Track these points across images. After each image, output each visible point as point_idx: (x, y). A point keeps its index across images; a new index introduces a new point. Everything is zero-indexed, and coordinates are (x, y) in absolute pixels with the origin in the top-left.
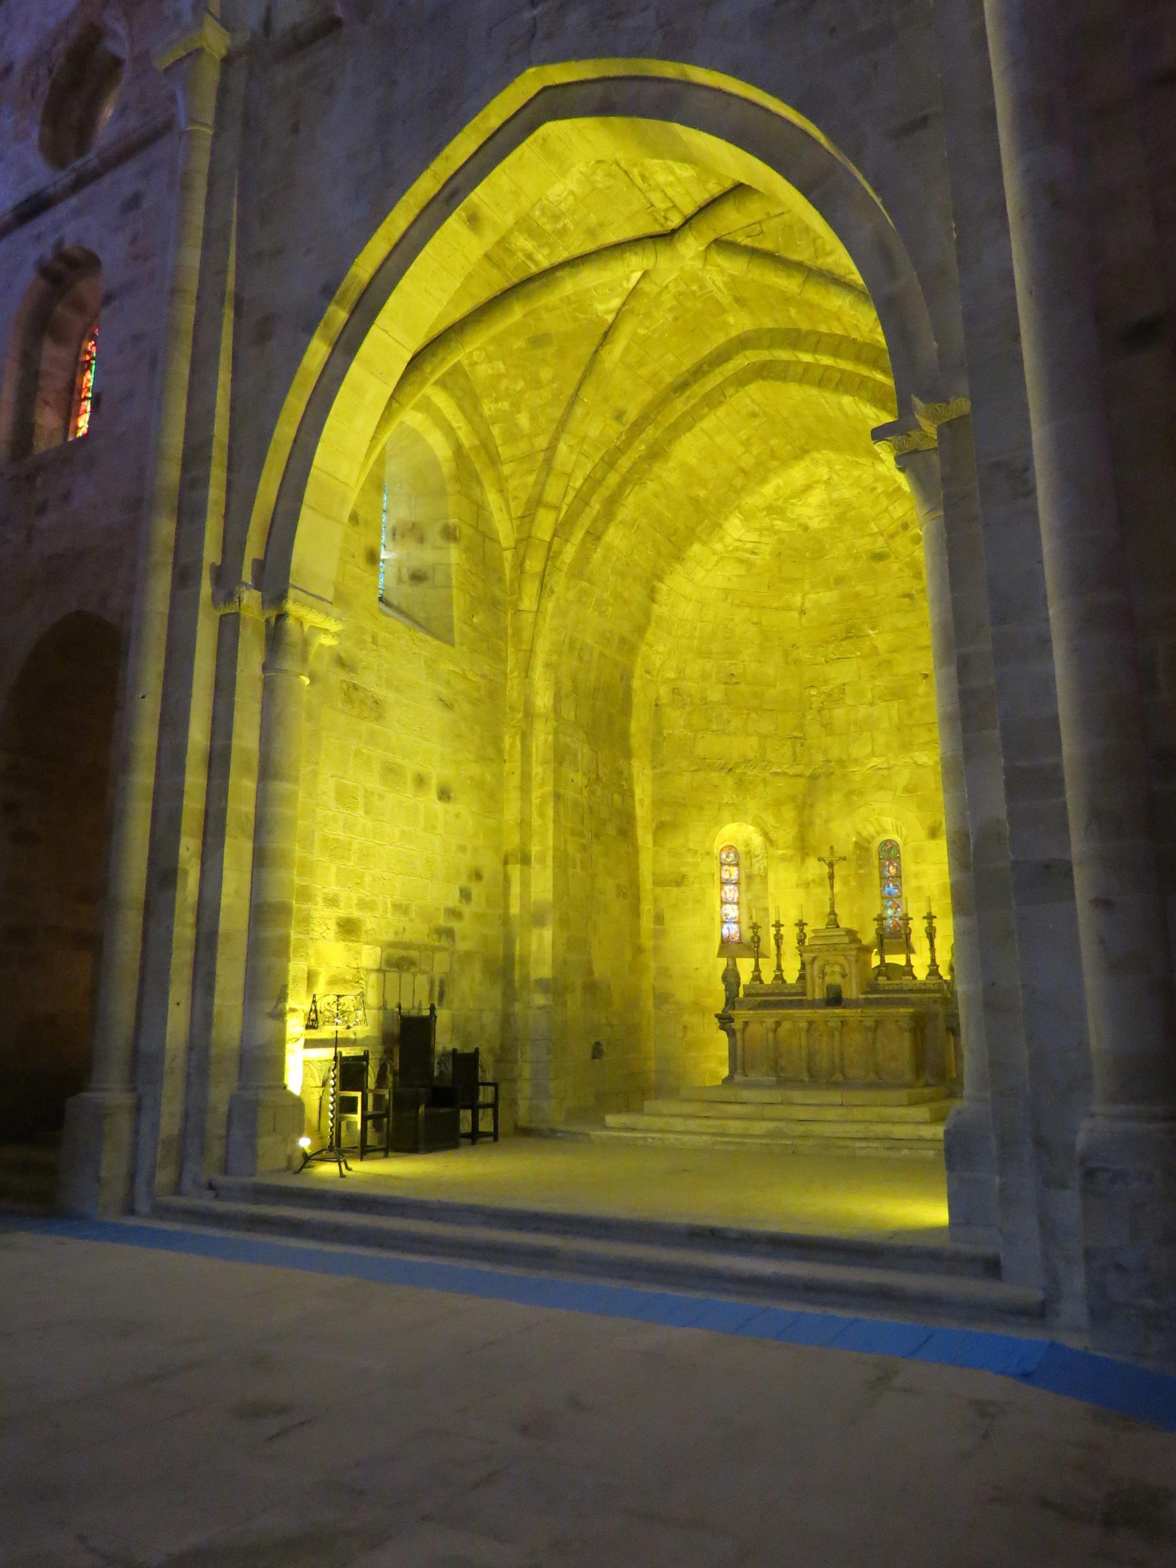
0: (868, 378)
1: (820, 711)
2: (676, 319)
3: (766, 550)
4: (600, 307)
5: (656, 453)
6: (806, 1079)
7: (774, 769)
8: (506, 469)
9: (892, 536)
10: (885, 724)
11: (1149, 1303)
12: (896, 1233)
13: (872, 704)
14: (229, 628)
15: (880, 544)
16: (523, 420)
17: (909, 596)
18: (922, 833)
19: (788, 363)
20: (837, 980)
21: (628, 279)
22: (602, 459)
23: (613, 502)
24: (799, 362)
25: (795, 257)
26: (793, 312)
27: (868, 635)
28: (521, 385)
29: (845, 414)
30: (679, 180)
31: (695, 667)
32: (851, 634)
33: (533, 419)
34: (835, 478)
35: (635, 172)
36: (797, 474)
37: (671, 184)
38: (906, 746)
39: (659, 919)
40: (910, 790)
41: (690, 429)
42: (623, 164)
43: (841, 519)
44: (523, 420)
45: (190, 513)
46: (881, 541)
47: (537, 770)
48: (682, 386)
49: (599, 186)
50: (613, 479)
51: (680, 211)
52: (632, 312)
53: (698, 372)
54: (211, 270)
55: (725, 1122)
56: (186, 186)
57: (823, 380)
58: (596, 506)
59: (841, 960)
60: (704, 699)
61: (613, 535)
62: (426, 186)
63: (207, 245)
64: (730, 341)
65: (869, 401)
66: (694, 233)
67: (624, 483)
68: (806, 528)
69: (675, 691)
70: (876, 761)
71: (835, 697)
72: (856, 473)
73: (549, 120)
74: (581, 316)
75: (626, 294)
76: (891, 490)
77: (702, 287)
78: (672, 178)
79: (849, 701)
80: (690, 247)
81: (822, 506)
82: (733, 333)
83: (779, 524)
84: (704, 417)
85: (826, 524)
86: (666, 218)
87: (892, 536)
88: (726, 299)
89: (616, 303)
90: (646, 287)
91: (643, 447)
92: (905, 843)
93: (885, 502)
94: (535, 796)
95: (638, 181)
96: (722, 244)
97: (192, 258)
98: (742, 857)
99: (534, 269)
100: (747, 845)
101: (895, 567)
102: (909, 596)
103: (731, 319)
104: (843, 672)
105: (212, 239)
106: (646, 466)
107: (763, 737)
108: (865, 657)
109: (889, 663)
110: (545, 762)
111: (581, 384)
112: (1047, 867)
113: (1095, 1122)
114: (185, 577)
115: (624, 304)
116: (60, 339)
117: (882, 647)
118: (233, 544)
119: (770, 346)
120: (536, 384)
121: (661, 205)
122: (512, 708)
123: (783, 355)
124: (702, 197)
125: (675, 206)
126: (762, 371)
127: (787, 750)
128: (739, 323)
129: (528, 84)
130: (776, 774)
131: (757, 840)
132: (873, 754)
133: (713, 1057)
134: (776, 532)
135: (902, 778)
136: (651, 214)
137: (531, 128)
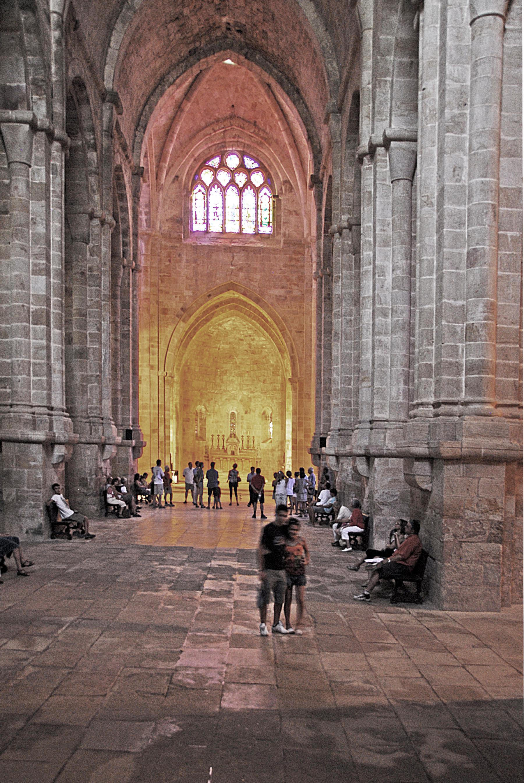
5: (207, 320)
10: (236, 382)
18: (244, 412)
20: (233, 450)
23: (196, 329)
32: (231, 357)
38: (241, 389)
40: (241, 401)
43: (234, 329)
67: (199, 325)
70: (233, 392)
81: (230, 324)
92: (238, 414)
107: (206, 382)
110: (176, 394)
117: (238, 362)
126: (236, 308)
135: (240, 398)
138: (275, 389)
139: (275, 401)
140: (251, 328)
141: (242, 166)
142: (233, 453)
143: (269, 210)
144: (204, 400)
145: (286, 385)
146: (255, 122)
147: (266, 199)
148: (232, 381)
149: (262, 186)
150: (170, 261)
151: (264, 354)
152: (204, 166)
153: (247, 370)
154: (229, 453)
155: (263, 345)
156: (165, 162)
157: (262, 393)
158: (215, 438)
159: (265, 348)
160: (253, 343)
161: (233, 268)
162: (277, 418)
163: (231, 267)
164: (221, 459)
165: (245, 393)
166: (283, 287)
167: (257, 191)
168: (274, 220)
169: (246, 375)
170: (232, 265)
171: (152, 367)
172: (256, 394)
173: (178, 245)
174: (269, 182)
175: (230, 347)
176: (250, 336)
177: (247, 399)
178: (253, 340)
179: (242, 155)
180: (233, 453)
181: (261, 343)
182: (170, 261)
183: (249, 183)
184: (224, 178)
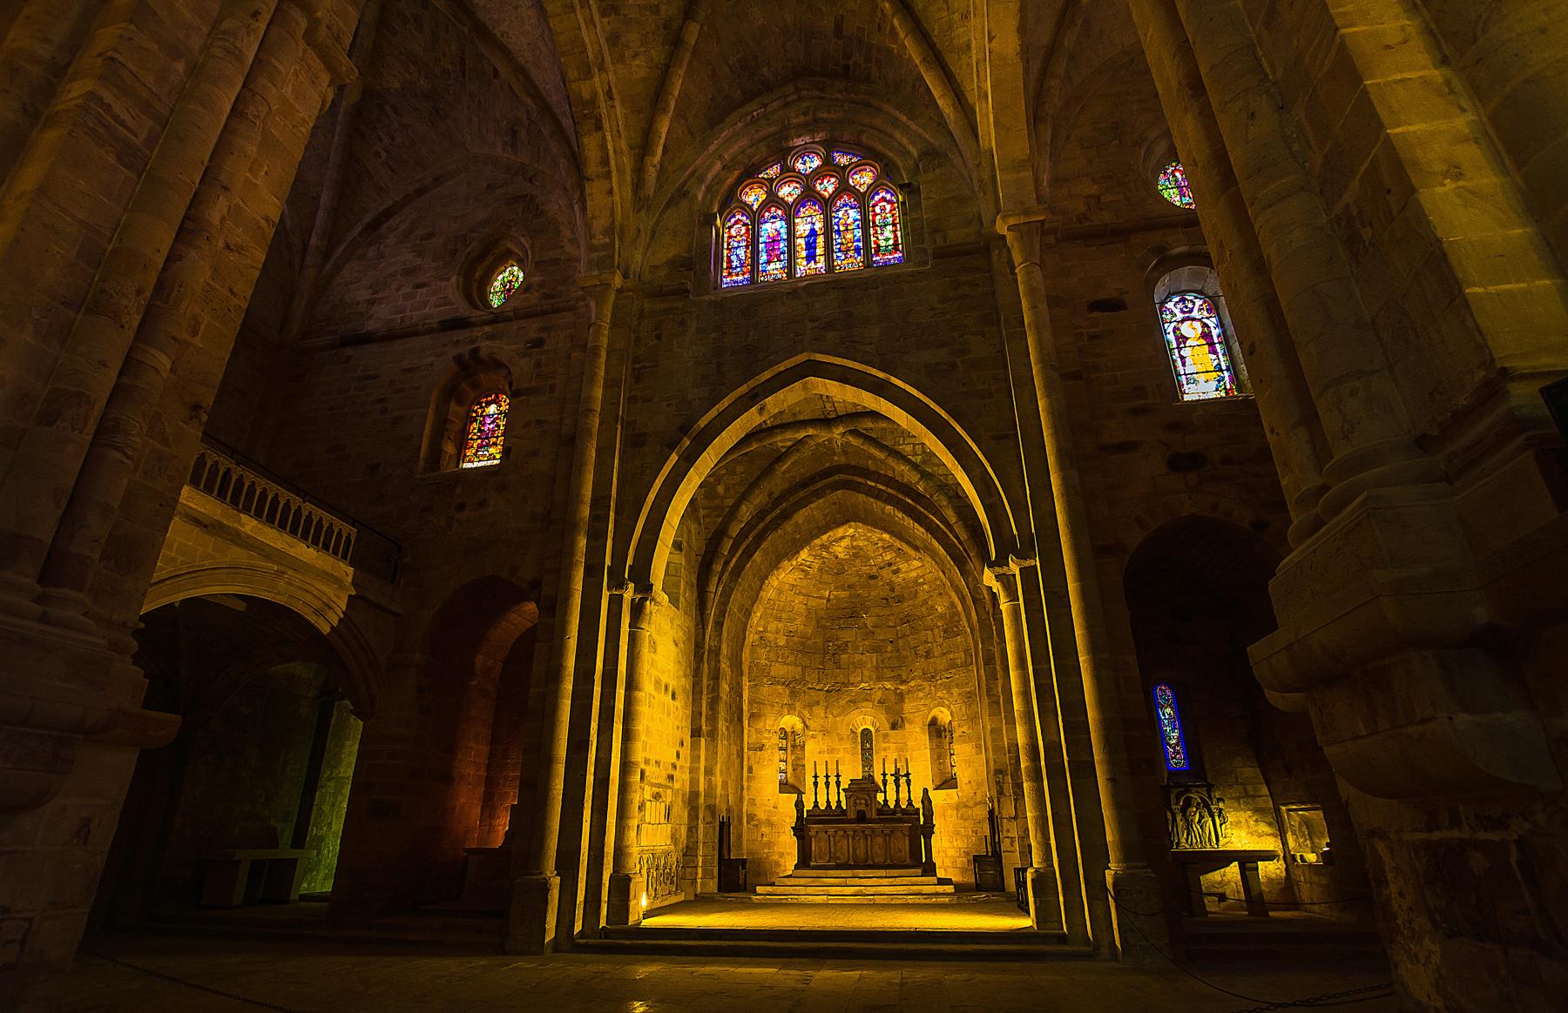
14: (616, 602)
16: (721, 489)
18: (888, 726)
20: (863, 807)
31: (772, 627)
32: (854, 615)
36: (840, 532)
38: (879, 679)
39: (750, 770)
44: (721, 489)
45: (597, 536)
50: (761, 525)
53: (813, 479)
54: (610, 402)
56: (597, 355)
57: (878, 496)
61: (757, 556)
71: (843, 648)
97: (598, 393)
104: (847, 636)
105: (609, 384)
114: (593, 571)
116: (460, 402)
118: (620, 557)
126: (847, 485)
127: (815, 675)
131: (799, 726)
133: (786, 849)
139: (955, 691)
140: (890, 547)
141: (828, 168)
143: (894, 225)
144: (798, 705)
146: (847, 67)
147: (885, 208)
148: (860, 665)
149: (874, 189)
150: (659, 337)
151: (922, 597)
152: (749, 174)
153: (891, 637)
156: (654, 154)
157: (925, 679)
160: (898, 579)
167: (863, 201)
168: (905, 235)
172: (912, 683)
173: (679, 304)
174: (887, 174)
175: (850, 596)
176: (890, 565)
177: (893, 697)
178: (896, 572)
179: (830, 146)
181: (913, 574)
182: (659, 337)
183: (844, 188)
184: (788, 192)
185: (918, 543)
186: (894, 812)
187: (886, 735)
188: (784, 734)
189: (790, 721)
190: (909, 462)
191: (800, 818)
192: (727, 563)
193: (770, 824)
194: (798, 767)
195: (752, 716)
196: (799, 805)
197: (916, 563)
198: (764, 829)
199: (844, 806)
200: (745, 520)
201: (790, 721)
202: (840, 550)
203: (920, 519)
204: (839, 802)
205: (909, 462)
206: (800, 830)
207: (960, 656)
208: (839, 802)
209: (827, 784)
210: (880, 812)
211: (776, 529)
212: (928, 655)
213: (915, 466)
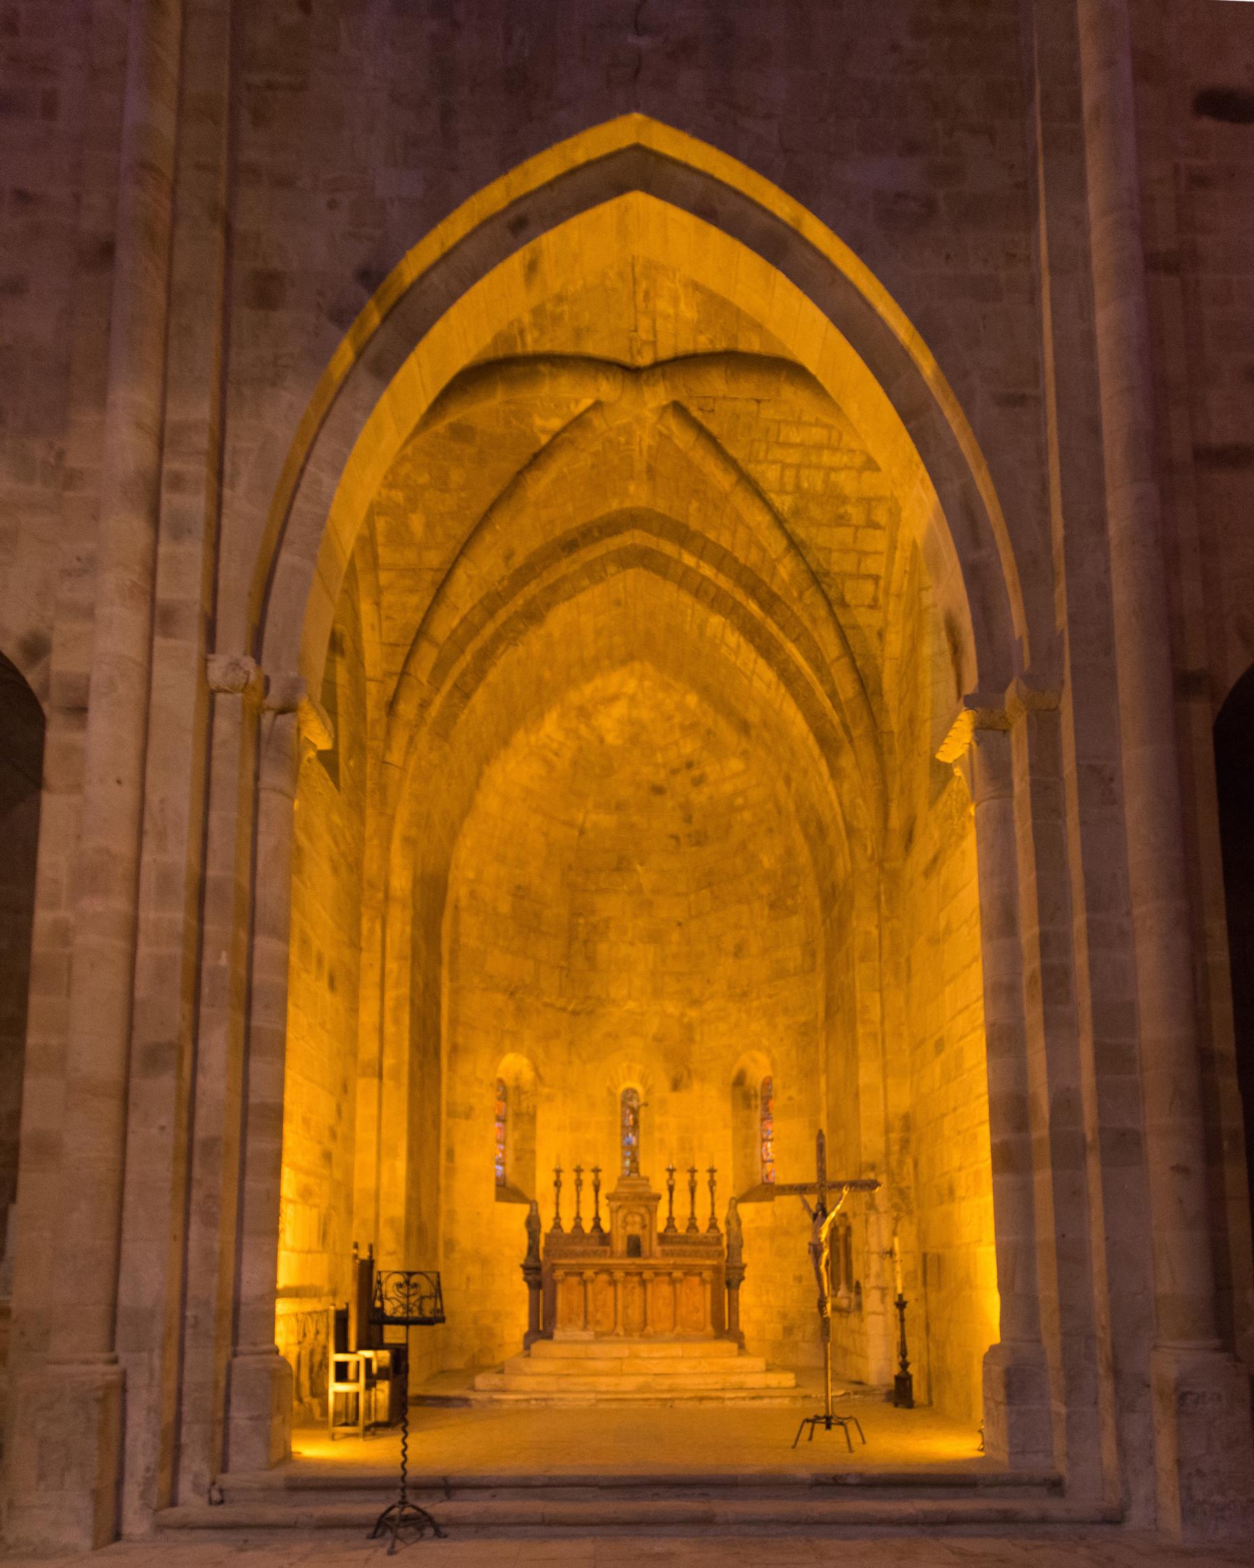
0: (740, 604)
1: (585, 942)
2: (593, 466)
3: (568, 754)
4: (538, 422)
5: (533, 615)
6: (622, 1333)
7: (547, 1000)
8: (384, 578)
9: (674, 772)
11: (1217, 1498)
12: (932, 1465)
13: (632, 944)
15: (661, 777)
16: (417, 522)
17: (676, 838)
19: (669, 558)
20: (635, 1230)
21: (577, 402)
22: (481, 602)
23: (486, 656)
24: (679, 562)
25: (732, 452)
26: (695, 505)
27: (635, 870)
28: (424, 479)
29: (702, 633)
30: (677, 315)
32: (621, 866)
33: (429, 526)
34: (640, 695)
35: (644, 285)
37: (667, 317)
38: (658, 993)
40: (658, 1039)
41: (569, 598)
42: (637, 269)
43: (634, 740)
44: (417, 522)
46: (663, 774)
47: (392, 966)
48: (570, 545)
49: (608, 283)
50: (489, 630)
51: (655, 353)
52: (572, 442)
55: (595, 1379)
57: (700, 590)
58: (467, 659)
59: (643, 1210)
60: (494, 908)
62: (495, 196)
63: (1089, 338)
64: (621, 512)
65: (738, 629)
66: (668, 384)
67: (498, 638)
68: (602, 740)
69: (473, 894)
70: (631, 1005)
72: (661, 695)
73: (642, 190)
74: (514, 422)
75: (570, 418)
76: (687, 723)
77: (628, 443)
78: (671, 311)
79: (612, 936)
80: (657, 395)
82: (627, 504)
83: (583, 730)
84: (583, 589)
85: (619, 742)
86: (639, 352)
87: (674, 772)
88: (640, 466)
89: (556, 424)
90: (598, 422)
91: (521, 602)
92: (649, 1092)
93: (677, 734)
94: (390, 995)
95: (640, 296)
96: (678, 408)
98: (511, 1092)
99: (519, 350)
100: (517, 1079)
101: (670, 804)
102: (676, 838)
103: (632, 488)
106: (521, 626)
108: (630, 893)
109: (651, 903)
111: (493, 507)
112: (1123, 1135)
113: (1170, 1358)
115: (564, 429)
119: (659, 535)
120: (442, 484)
121: (644, 335)
122: (372, 886)
123: (669, 548)
124: (686, 345)
125: (654, 343)
126: (644, 558)
128: (637, 495)
129: (628, 130)
130: (546, 1005)
131: (528, 1075)
132: (629, 996)
134: (579, 738)
136: (631, 340)
137: (620, 189)
138: (780, 973)
139: (781, 1021)
142: (635, 1247)
145: (949, 726)
154: (620, 1245)
155: (736, 794)
158: (568, 1179)
159: (741, 809)
160: (700, 797)
161: (645, 42)
162: (793, 1092)
163: (632, 39)
164: (589, 1273)
165: (672, 1008)
166: (911, 148)
169: (675, 937)
170: (639, 29)
171: (160, 619)
172: (709, 1006)
176: (689, 765)
178: (698, 782)
180: (635, 1247)
181: (728, 788)
185: (753, 716)
186: (684, 1240)
187: (663, 1102)
188: (502, 1091)
189: (514, 1065)
190: (768, 506)
191: (533, 1249)
192: (424, 705)
193: (484, 1262)
194: (525, 1155)
195: (454, 1048)
196: (533, 1224)
197: (736, 765)
198: (473, 1269)
199: (606, 1226)
200: (465, 608)
201: (514, 1065)
202: (610, 723)
203: (768, 650)
204: (597, 1219)
205: (768, 506)
206: (535, 1273)
207: (793, 955)
208: (597, 1219)
209: (579, 1183)
210: (662, 1238)
211: (514, 642)
212: (739, 952)
213: (779, 521)
